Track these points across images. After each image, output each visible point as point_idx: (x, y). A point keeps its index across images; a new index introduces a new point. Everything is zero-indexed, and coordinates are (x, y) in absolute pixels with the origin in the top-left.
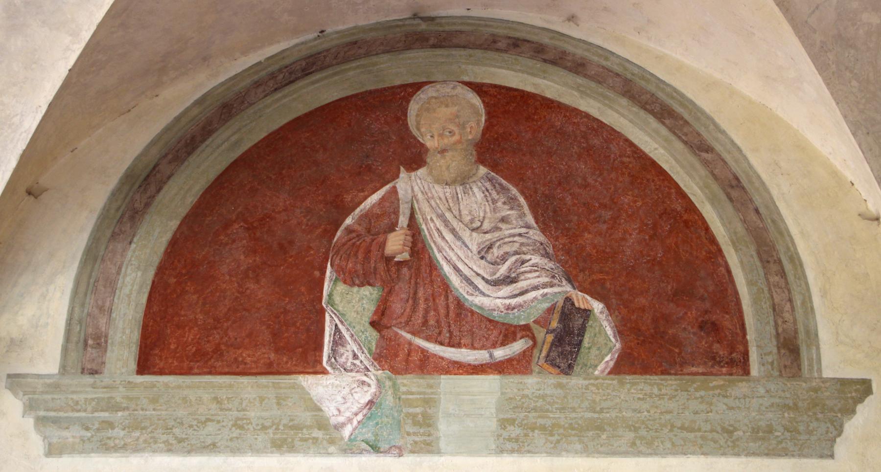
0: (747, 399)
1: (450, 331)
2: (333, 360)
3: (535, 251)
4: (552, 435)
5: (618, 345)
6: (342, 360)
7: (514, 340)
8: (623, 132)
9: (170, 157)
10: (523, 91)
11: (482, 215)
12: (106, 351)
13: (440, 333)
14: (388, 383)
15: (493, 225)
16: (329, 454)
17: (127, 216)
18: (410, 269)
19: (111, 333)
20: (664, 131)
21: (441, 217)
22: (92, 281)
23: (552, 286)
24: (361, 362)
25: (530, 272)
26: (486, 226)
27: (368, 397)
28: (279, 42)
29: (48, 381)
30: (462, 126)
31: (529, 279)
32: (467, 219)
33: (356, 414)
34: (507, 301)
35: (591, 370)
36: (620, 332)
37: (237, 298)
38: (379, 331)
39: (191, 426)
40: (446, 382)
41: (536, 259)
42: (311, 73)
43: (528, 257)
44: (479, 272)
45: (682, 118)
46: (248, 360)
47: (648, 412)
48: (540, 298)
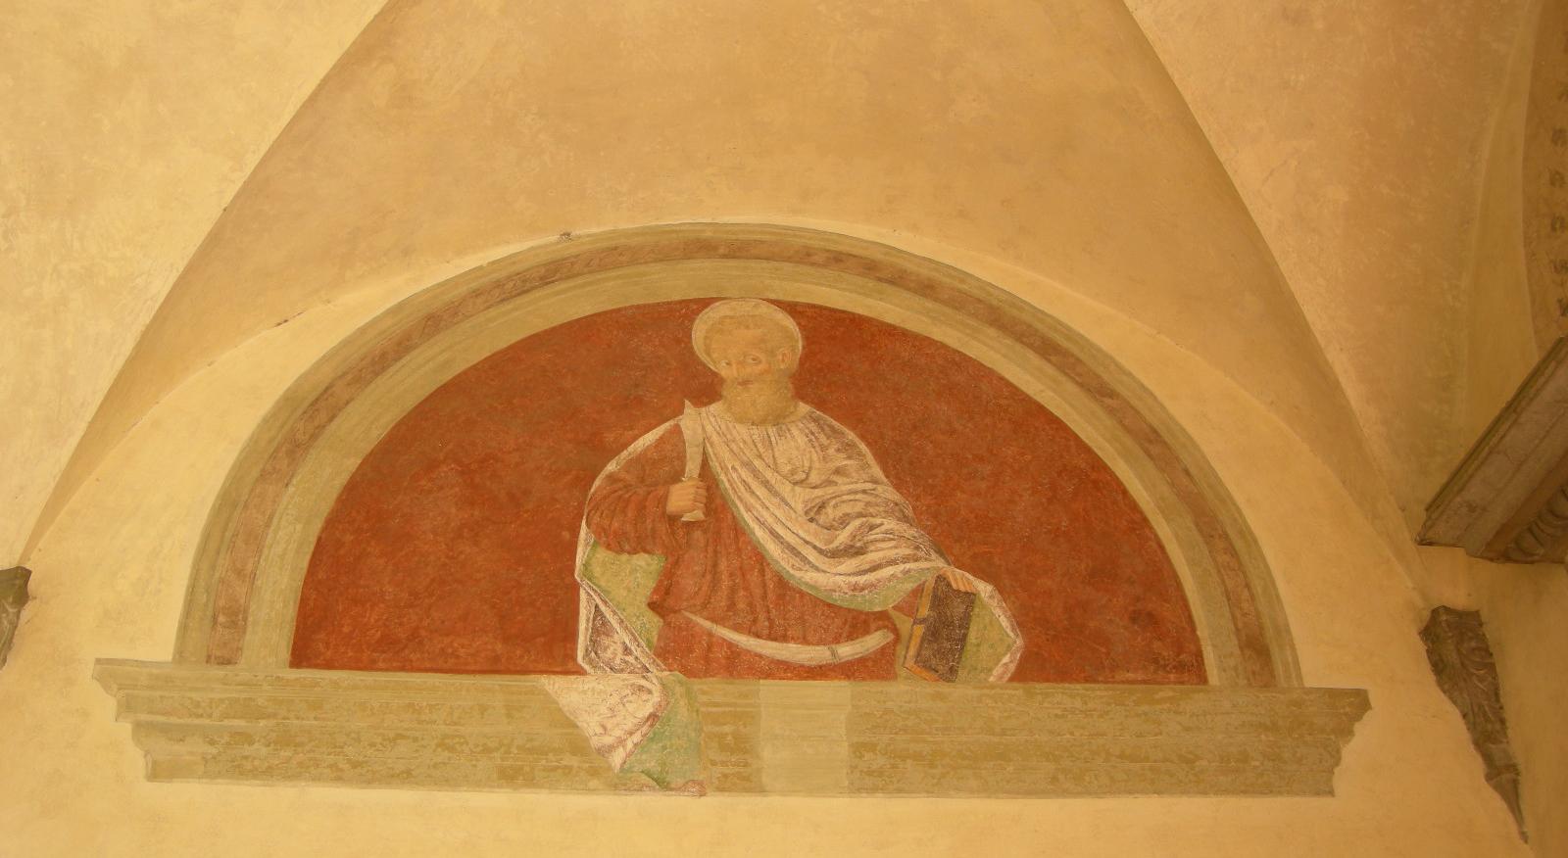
0: (1208, 717)
1: (769, 619)
2: (593, 654)
3: (888, 514)
4: (932, 765)
5: (1020, 642)
6: (609, 654)
7: (867, 632)
8: (995, 368)
9: (349, 377)
10: (853, 314)
11: (807, 464)
12: (244, 632)
13: (755, 621)
14: (678, 689)
15: (823, 477)
16: (593, 791)
17: (284, 449)
18: (705, 532)
19: (253, 607)
20: (1050, 370)
21: (748, 465)
22: (228, 534)
23: (916, 561)
24: (636, 658)
25: (883, 540)
26: (814, 478)
27: (648, 709)
28: (508, 243)
29: (155, 671)
30: (772, 353)
31: (882, 549)
32: (786, 469)
33: (631, 734)
34: (853, 579)
35: (983, 675)
36: (1021, 623)
37: (444, 565)
38: (662, 616)
39: (372, 745)
40: (770, 691)
41: (890, 524)
42: (553, 282)
43: (878, 521)
44: (808, 539)
45: (1073, 355)
46: (462, 652)
47: (1072, 734)
48: (900, 575)
